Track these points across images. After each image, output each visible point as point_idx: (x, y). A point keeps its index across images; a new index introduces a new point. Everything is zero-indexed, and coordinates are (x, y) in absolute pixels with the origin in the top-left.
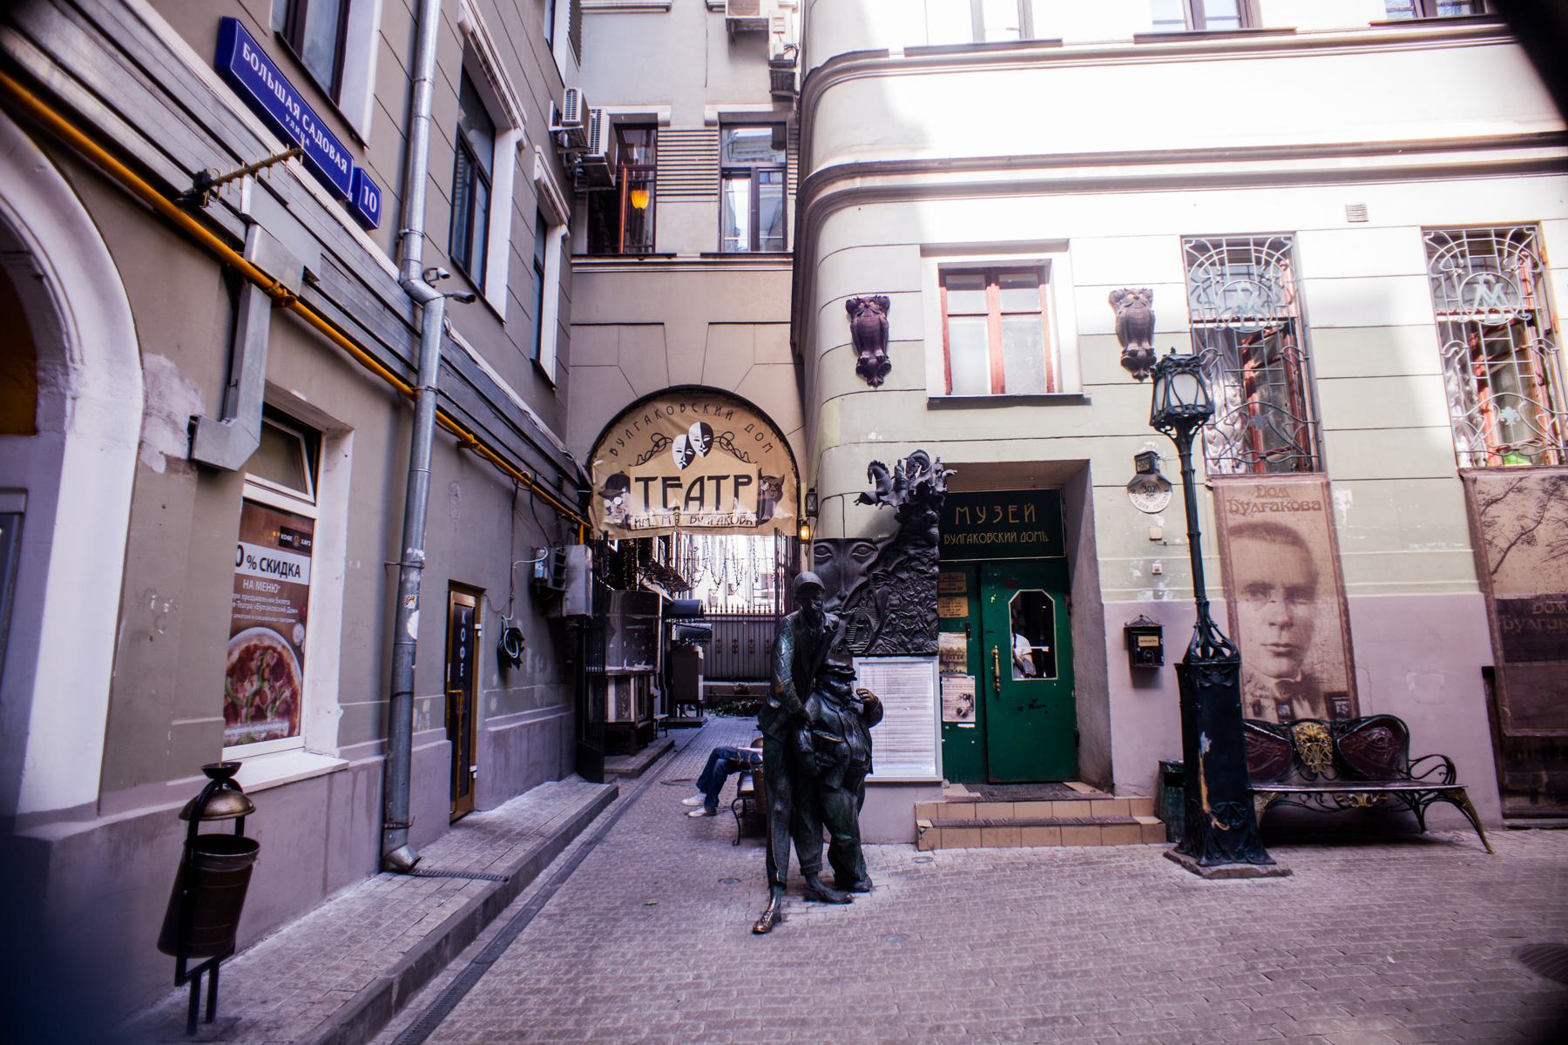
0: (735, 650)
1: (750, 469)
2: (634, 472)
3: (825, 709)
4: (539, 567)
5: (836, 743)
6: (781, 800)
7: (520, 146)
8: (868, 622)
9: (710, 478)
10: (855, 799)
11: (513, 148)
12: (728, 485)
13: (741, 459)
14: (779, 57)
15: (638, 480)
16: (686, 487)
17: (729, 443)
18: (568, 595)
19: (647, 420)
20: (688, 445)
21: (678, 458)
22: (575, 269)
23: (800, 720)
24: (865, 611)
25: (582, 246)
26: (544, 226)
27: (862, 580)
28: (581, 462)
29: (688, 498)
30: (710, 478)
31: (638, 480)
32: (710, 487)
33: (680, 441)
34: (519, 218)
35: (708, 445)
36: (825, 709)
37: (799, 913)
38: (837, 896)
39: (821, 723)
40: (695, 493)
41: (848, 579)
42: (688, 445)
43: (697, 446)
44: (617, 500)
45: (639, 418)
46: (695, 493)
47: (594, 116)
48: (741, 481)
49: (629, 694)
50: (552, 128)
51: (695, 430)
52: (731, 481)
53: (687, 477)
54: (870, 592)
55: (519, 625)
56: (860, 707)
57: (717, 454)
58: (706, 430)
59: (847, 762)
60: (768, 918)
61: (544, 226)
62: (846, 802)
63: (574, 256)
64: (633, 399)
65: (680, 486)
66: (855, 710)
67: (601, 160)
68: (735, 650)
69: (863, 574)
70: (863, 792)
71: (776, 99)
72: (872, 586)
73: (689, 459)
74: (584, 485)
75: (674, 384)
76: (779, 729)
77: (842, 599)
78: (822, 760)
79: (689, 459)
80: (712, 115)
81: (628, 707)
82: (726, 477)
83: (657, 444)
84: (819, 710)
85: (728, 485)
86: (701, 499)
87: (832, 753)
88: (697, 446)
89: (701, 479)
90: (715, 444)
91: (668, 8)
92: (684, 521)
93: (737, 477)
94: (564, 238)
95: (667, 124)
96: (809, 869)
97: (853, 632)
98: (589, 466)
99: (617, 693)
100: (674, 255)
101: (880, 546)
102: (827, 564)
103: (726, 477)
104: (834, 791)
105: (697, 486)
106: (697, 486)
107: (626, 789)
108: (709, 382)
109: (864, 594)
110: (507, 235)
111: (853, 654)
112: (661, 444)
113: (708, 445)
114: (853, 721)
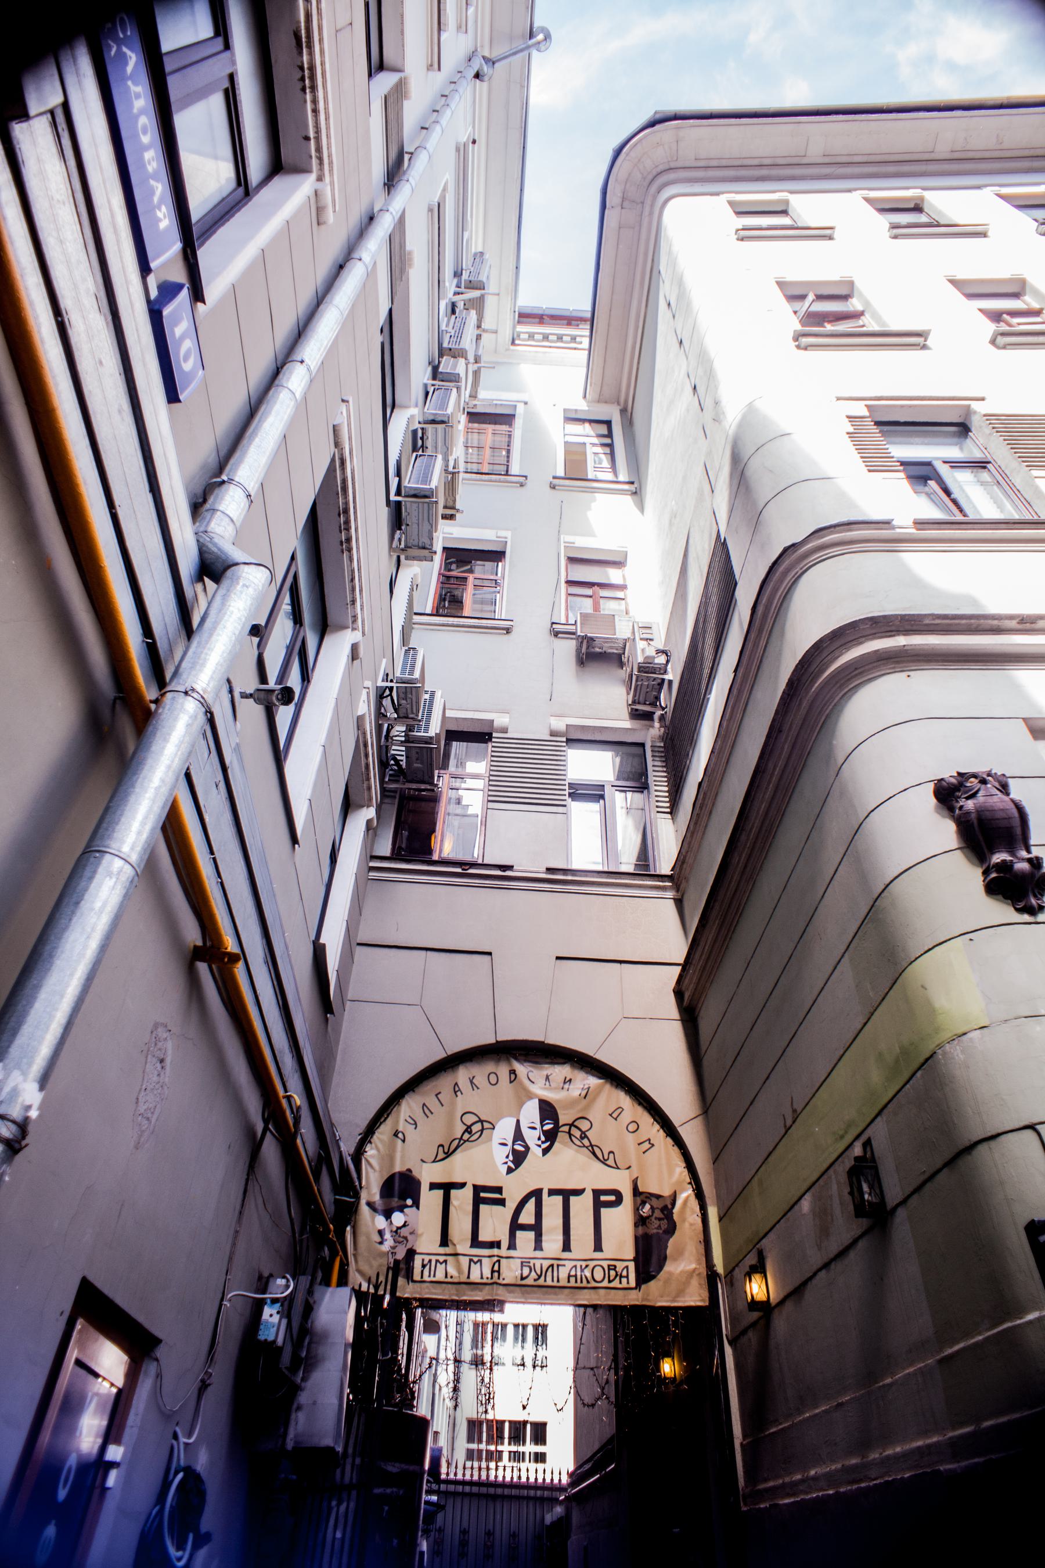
0: (464, 1543)
1: (621, 1181)
2: (428, 1174)
4: (271, 1315)
7: (355, 648)
9: (552, 1192)
11: (347, 650)
12: (582, 1208)
13: (604, 1162)
14: (649, 660)
15: (433, 1186)
16: (511, 1205)
17: (584, 1136)
18: (303, 1398)
19: (456, 1090)
20: (518, 1136)
21: (501, 1156)
22: (373, 874)
25: (385, 847)
26: (348, 806)
28: (347, 1147)
29: (515, 1226)
30: (552, 1192)
31: (433, 1186)
32: (552, 1206)
33: (505, 1129)
35: (551, 1137)
40: (527, 1217)
42: (518, 1136)
43: (532, 1137)
44: (398, 1218)
45: (444, 1083)
46: (527, 1217)
47: (427, 696)
48: (604, 1200)
50: (380, 684)
51: (531, 1113)
52: (588, 1198)
53: (514, 1189)
55: (202, 1462)
57: (565, 1152)
58: (548, 1110)
61: (348, 806)
63: (373, 858)
64: (439, 1055)
65: (502, 1202)
67: (429, 740)
68: (464, 1543)
71: (636, 715)
73: (519, 1158)
74: (348, 1186)
75: (504, 1036)
79: (519, 1158)
80: (559, 724)
82: (578, 1192)
83: (468, 1130)
85: (582, 1208)
86: (537, 1228)
88: (532, 1137)
89: (537, 1194)
90: (562, 1136)
91: (508, 631)
92: (511, 1272)
93: (597, 1193)
94: (369, 822)
95: (505, 730)
98: (358, 1155)
100: (510, 868)
103: (578, 1192)
105: (531, 1205)
106: (531, 1205)
108: (552, 1040)
110: (322, 738)
112: (476, 1129)
113: (551, 1137)
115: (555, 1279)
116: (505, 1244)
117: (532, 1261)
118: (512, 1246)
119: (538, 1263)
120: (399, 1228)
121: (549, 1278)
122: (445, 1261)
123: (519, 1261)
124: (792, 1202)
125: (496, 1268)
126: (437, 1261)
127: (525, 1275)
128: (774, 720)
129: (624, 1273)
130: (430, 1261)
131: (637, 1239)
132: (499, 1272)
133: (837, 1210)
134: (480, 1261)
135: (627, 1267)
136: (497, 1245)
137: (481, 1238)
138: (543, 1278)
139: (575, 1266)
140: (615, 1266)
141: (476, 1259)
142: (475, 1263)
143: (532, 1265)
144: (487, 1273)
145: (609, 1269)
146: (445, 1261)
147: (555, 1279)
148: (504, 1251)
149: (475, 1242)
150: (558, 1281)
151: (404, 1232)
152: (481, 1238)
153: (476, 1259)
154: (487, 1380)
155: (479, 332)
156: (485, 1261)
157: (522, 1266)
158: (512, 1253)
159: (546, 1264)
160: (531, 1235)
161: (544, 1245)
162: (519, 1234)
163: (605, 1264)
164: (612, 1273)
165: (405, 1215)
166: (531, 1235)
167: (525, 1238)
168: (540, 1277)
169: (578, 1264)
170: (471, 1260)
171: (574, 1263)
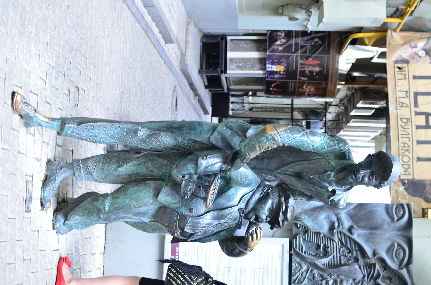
3: (243, 191)
5: (205, 199)
6: (150, 136)
8: (326, 255)
10: (146, 220)
23: (232, 158)
24: (336, 253)
27: (369, 252)
34: (392, 216)
36: (243, 191)
37: (36, 149)
38: (51, 193)
39: (227, 184)
41: (369, 239)
49: (250, 69)
54: (356, 260)
56: (241, 232)
59: (185, 212)
60: (28, 110)
62: (143, 209)
66: (239, 226)
69: (374, 253)
70: (153, 231)
72: (363, 261)
76: (224, 139)
77: (350, 230)
78: (188, 181)
81: (238, 67)
84: (240, 184)
87: (194, 195)
96: (78, 165)
97: (315, 240)
99: (249, 60)
101: (404, 272)
102: (386, 217)
104: (156, 195)
107: (172, 50)
109: (354, 254)
111: (293, 238)
114: (227, 222)
115: (402, 136)
116: (417, 110)
117: (410, 124)
118: (417, 114)
119: (409, 127)
120: (417, 54)
121: (403, 133)
122: (406, 79)
123: (409, 117)
124: (281, 255)
125: (404, 105)
126: (405, 75)
127: (403, 120)
128: (141, 230)
129: (407, 173)
130: (405, 71)
131: (424, 181)
132: (402, 106)
133: (74, 264)
134: (407, 97)
135: (410, 174)
136: (416, 105)
137: (419, 97)
138: (402, 129)
139: (409, 147)
140: (410, 168)
141: (408, 94)
142: (406, 94)
143: (408, 123)
144: (402, 100)
145: (408, 165)
146: (406, 79)
147: (402, 136)
148: (414, 109)
149: (416, 94)
150: (402, 137)
151: (416, 57)
152: (419, 97)
153: (408, 94)
154: (124, 77)
155: (295, 4)
156: (408, 99)
157: (407, 119)
158: (413, 114)
159: (409, 131)
160: (424, 123)
161: (419, 130)
162: (423, 117)
163: (410, 163)
164: (406, 167)
165: (425, 57)
166: (424, 123)
167: (421, 120)
168: (403, 128)
169: (411, 148)
170: (407, 92)
171: (411, 146)
